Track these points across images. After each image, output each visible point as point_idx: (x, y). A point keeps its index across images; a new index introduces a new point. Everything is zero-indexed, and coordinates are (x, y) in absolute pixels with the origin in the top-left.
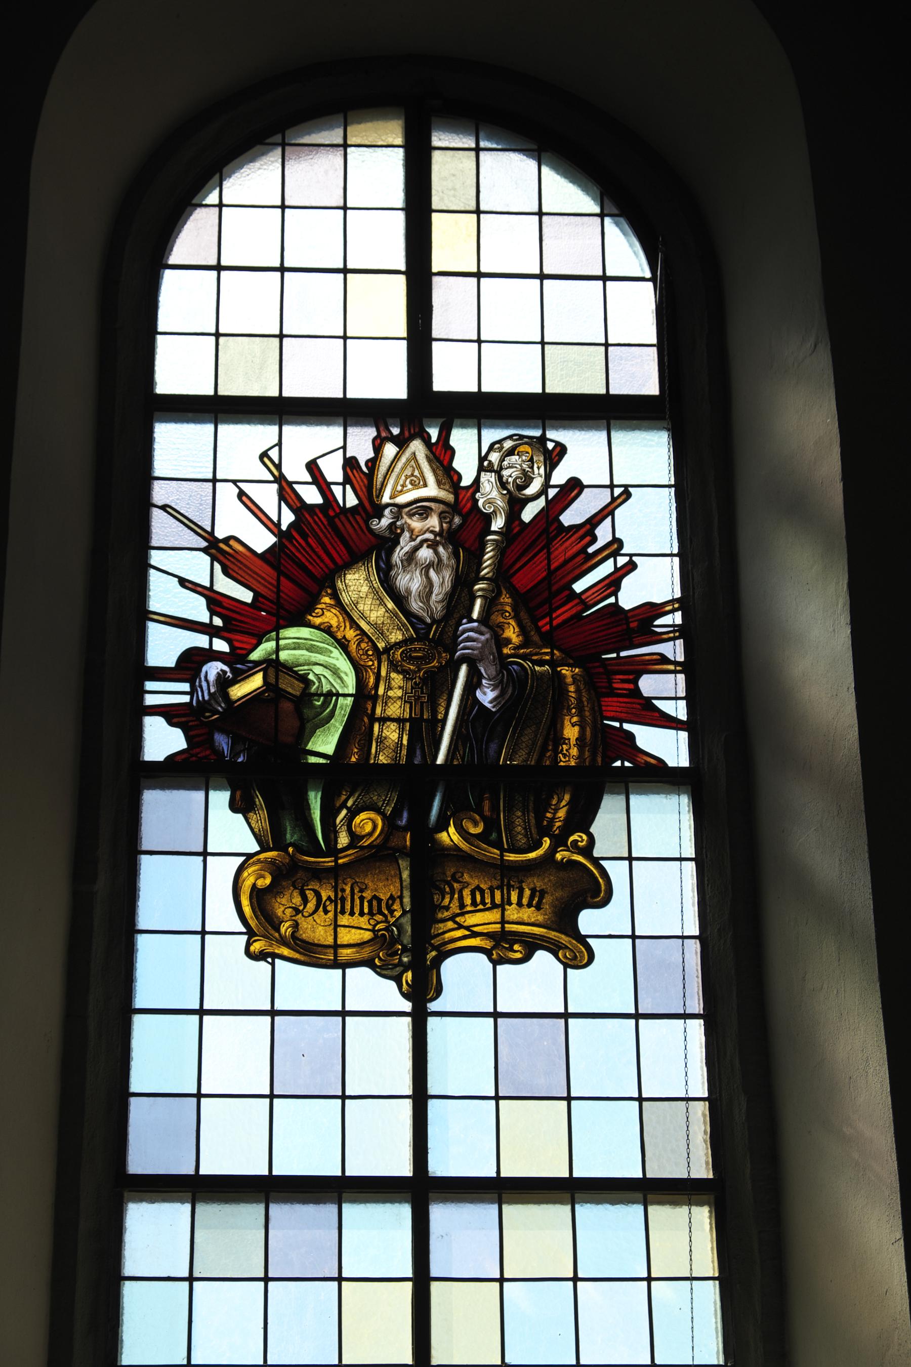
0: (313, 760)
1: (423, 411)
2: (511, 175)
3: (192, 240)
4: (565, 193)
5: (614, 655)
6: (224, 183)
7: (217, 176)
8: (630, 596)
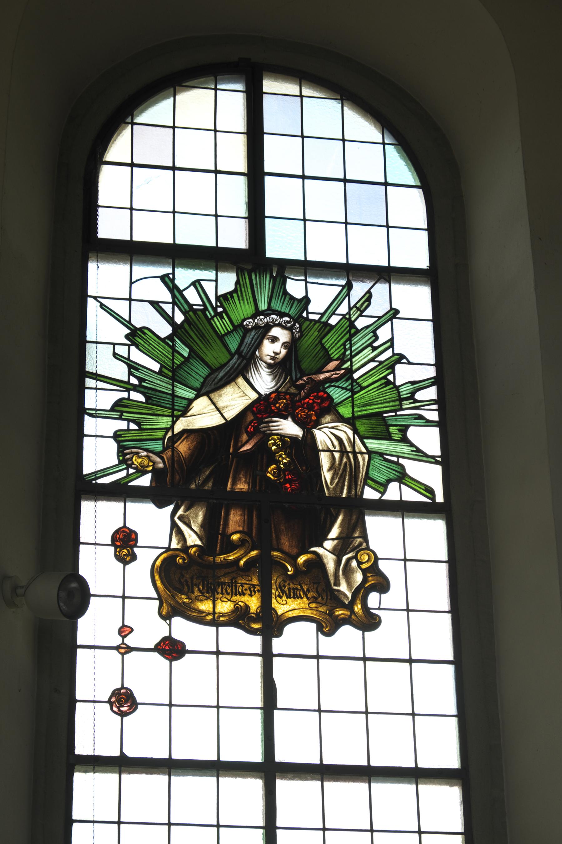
0: (237, 490)
1: (251, 261)
2: (324, 112)
3: (118, 149)
4: (361, 127)
5: (393, 414)
6: (393, 147)
7: (396, 143)
8: (403, 375)
